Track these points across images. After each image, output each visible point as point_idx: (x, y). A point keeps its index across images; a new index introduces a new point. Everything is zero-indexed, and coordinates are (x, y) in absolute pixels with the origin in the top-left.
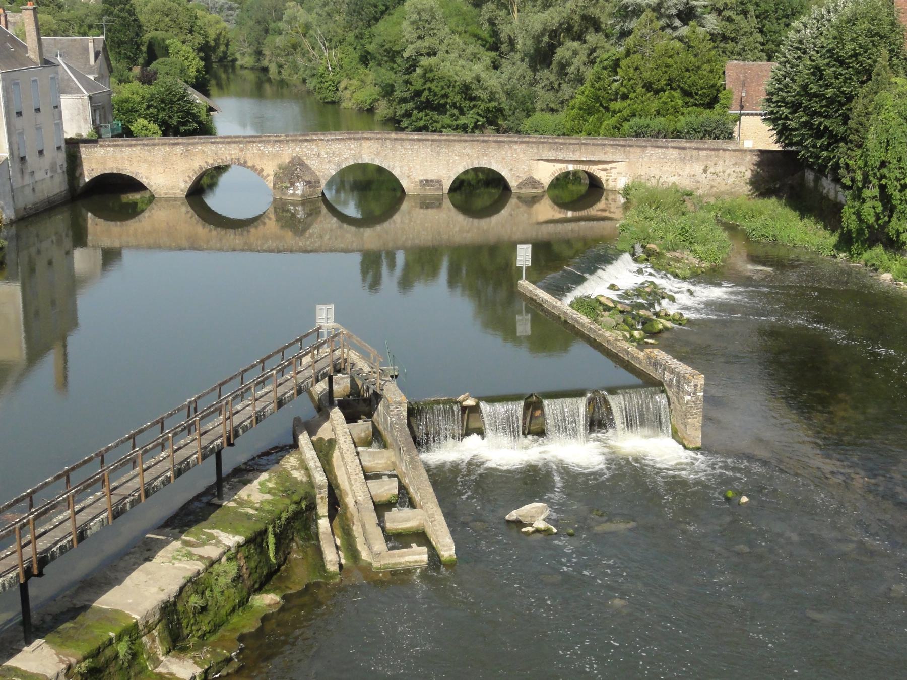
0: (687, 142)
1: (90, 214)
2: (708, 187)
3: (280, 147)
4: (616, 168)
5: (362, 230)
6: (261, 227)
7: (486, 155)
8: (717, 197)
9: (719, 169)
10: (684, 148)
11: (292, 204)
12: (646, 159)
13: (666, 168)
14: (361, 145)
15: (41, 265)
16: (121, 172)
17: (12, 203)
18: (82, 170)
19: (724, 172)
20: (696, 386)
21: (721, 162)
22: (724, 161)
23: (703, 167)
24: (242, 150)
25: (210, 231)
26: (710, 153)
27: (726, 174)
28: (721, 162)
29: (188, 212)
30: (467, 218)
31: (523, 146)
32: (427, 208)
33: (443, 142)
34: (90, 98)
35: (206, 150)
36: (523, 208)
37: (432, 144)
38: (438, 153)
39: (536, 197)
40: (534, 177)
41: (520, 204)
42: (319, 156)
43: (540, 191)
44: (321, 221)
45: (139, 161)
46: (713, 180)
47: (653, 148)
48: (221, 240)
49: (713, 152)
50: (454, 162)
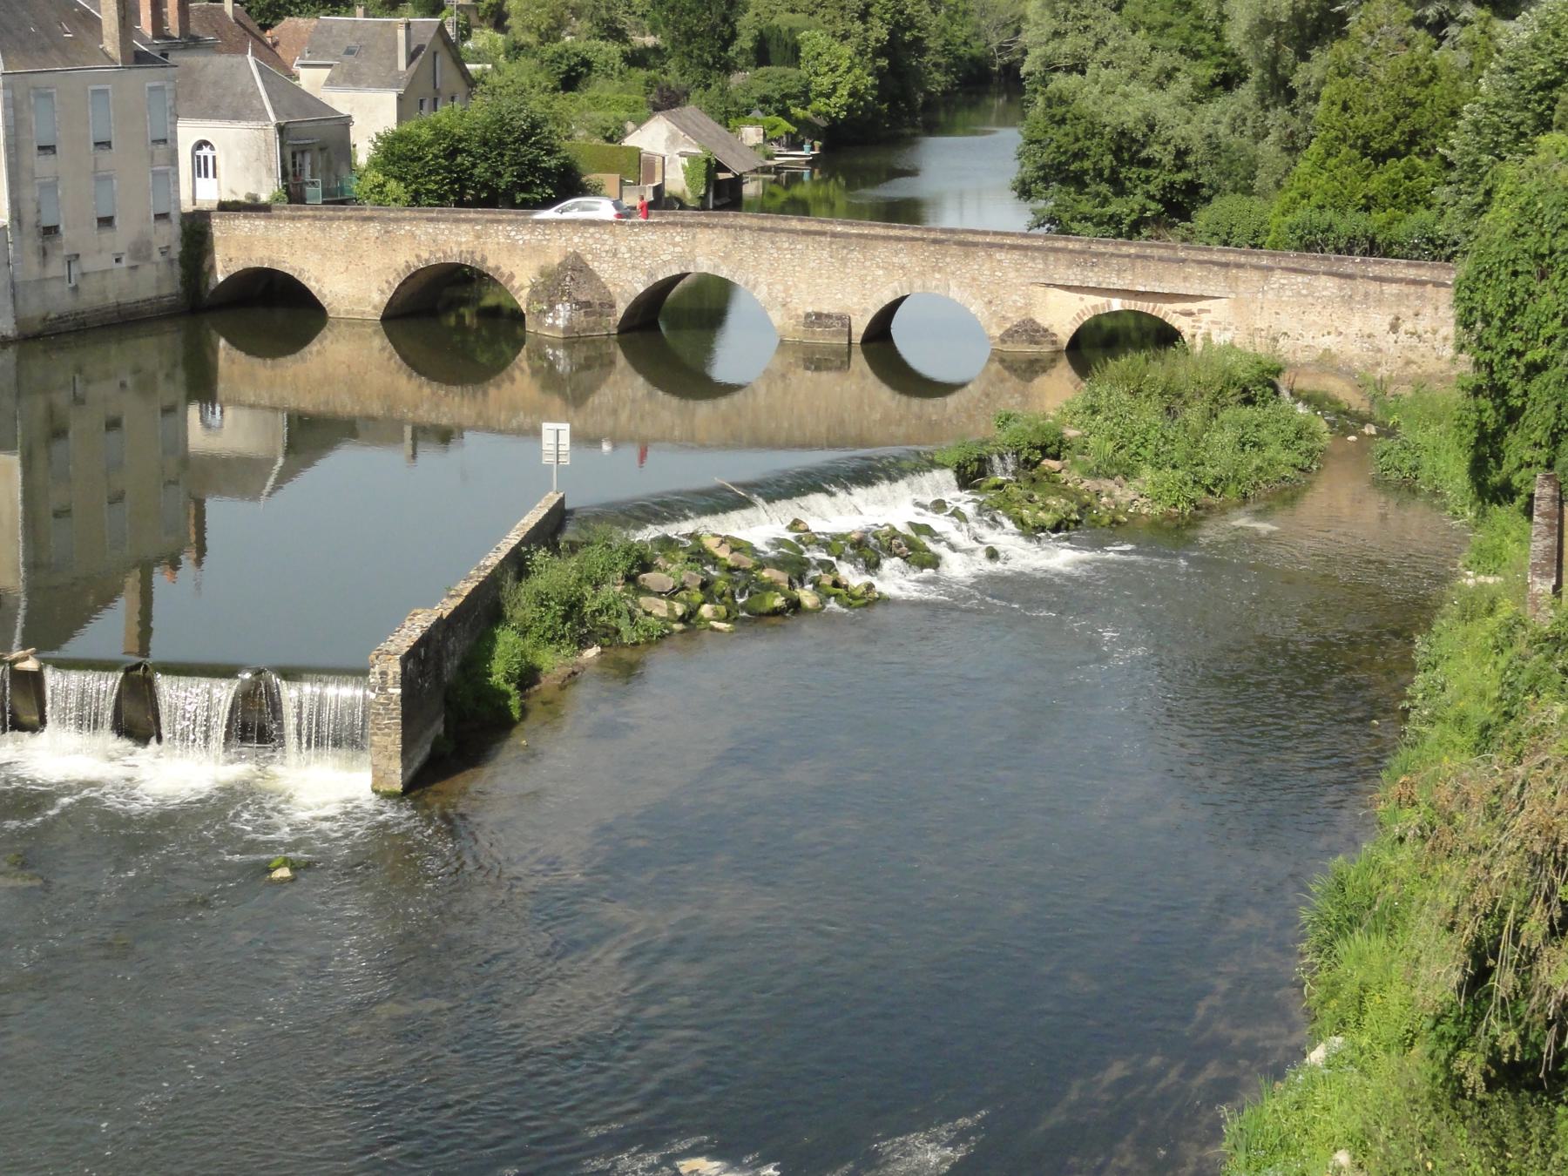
0: (1408, 265)
1: (222, 342)
2: (1400, 363)
3: (545, 234)
4: (1209, 311)
5: (691, 403)
6: (507, 385)
7: (940, 270)
8: (1419, 384)
9: (1423, 325)
10: (1351, 277)
11: (552, 345)
12: (1270, 295)
13: (1313, 317)
14: (694, 238)
15: (83, 425)
16: (275, 267)
17: (10, 307)
18: (213, 259)
19: (1435, 332)
20: (383, 674)
21: (1429, 311)
22: (1436, 309)
23: (1390, 319)
24: (478, 237)
25: (420, 387)
26: (1405, 289)
27: (1439, 337)
28: (1429, 311)
29: (383, 349)
30: (898, 396)
31: (1016, 255)
32: (818, 369)
33: (854, 240)
34: (281, 130)
35: (418, 232)
36: (1013, 381)
37: (831, 243)
38: (844, 262)
39: (1037, 360)
40: (1039, 320)
41: (1006, 374)
42: (615, 255)
43: (1047, 349)
44: (616, 382)
45: (305, 248)
46: (1412, 349)
47: (1286, 274)
48: (437, 406)
49: (1412, 288)
50: (874, 280)
